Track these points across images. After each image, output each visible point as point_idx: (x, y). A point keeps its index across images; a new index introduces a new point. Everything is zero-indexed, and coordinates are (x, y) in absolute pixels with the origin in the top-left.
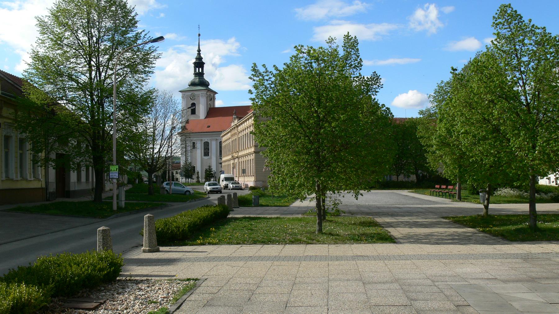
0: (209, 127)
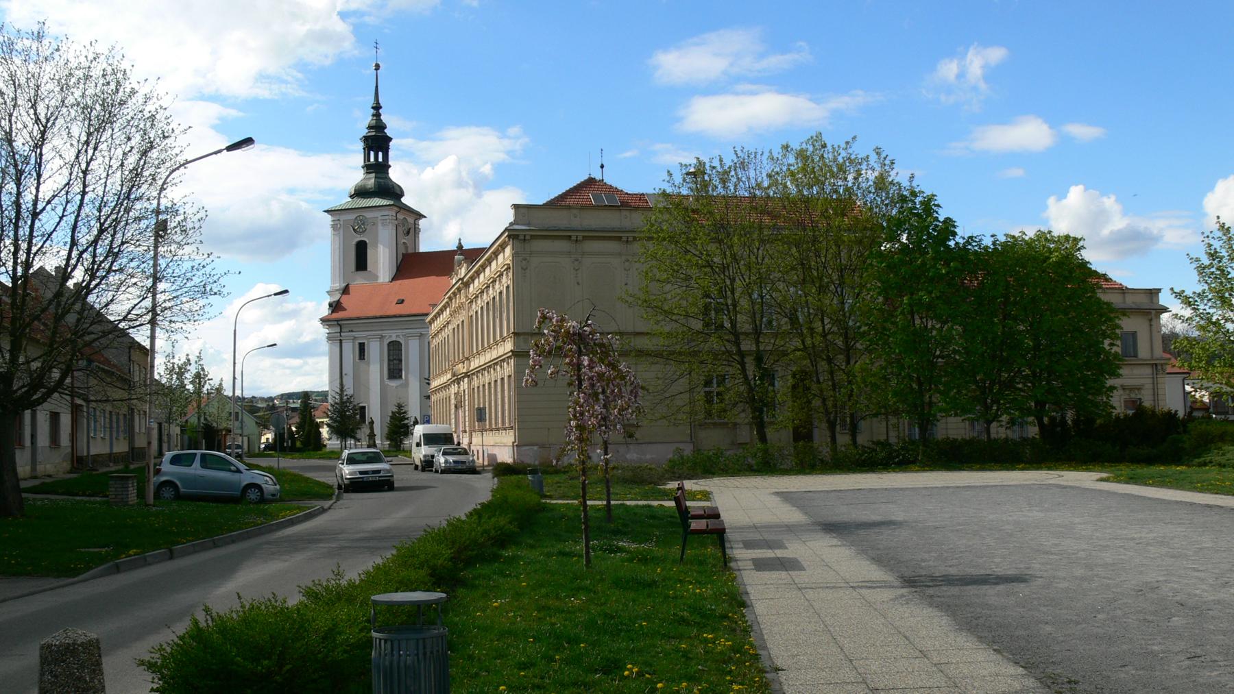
0: (402, 302)
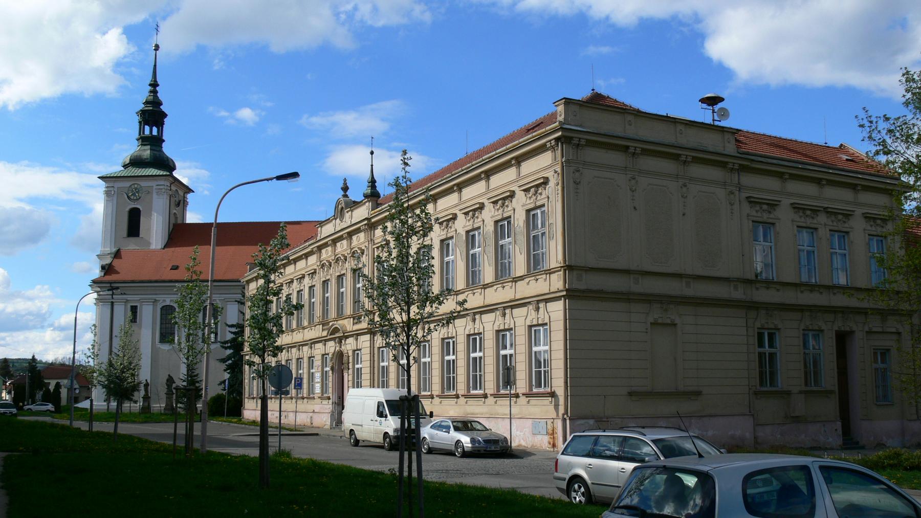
0: (175, 268)
